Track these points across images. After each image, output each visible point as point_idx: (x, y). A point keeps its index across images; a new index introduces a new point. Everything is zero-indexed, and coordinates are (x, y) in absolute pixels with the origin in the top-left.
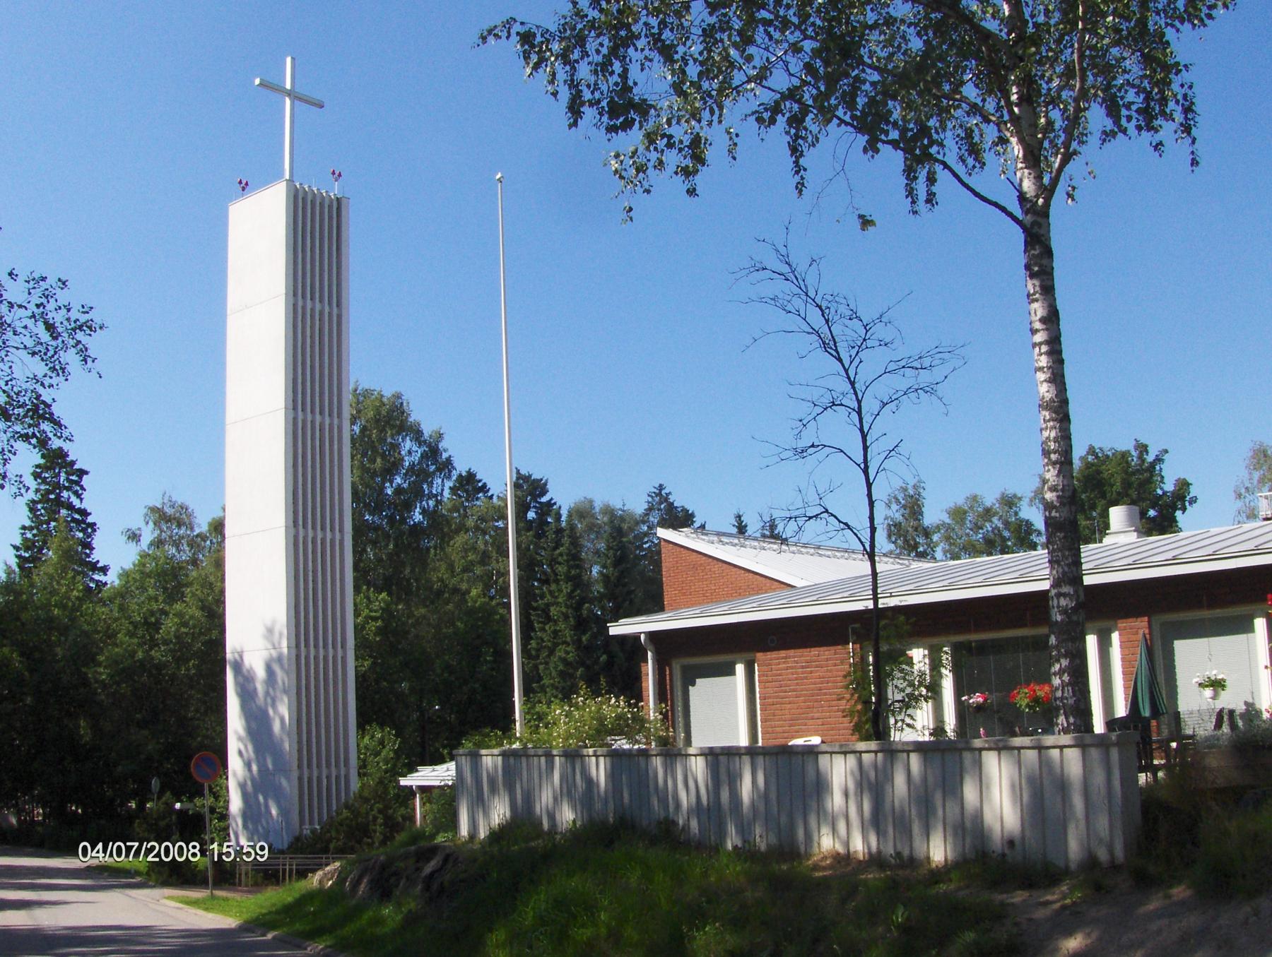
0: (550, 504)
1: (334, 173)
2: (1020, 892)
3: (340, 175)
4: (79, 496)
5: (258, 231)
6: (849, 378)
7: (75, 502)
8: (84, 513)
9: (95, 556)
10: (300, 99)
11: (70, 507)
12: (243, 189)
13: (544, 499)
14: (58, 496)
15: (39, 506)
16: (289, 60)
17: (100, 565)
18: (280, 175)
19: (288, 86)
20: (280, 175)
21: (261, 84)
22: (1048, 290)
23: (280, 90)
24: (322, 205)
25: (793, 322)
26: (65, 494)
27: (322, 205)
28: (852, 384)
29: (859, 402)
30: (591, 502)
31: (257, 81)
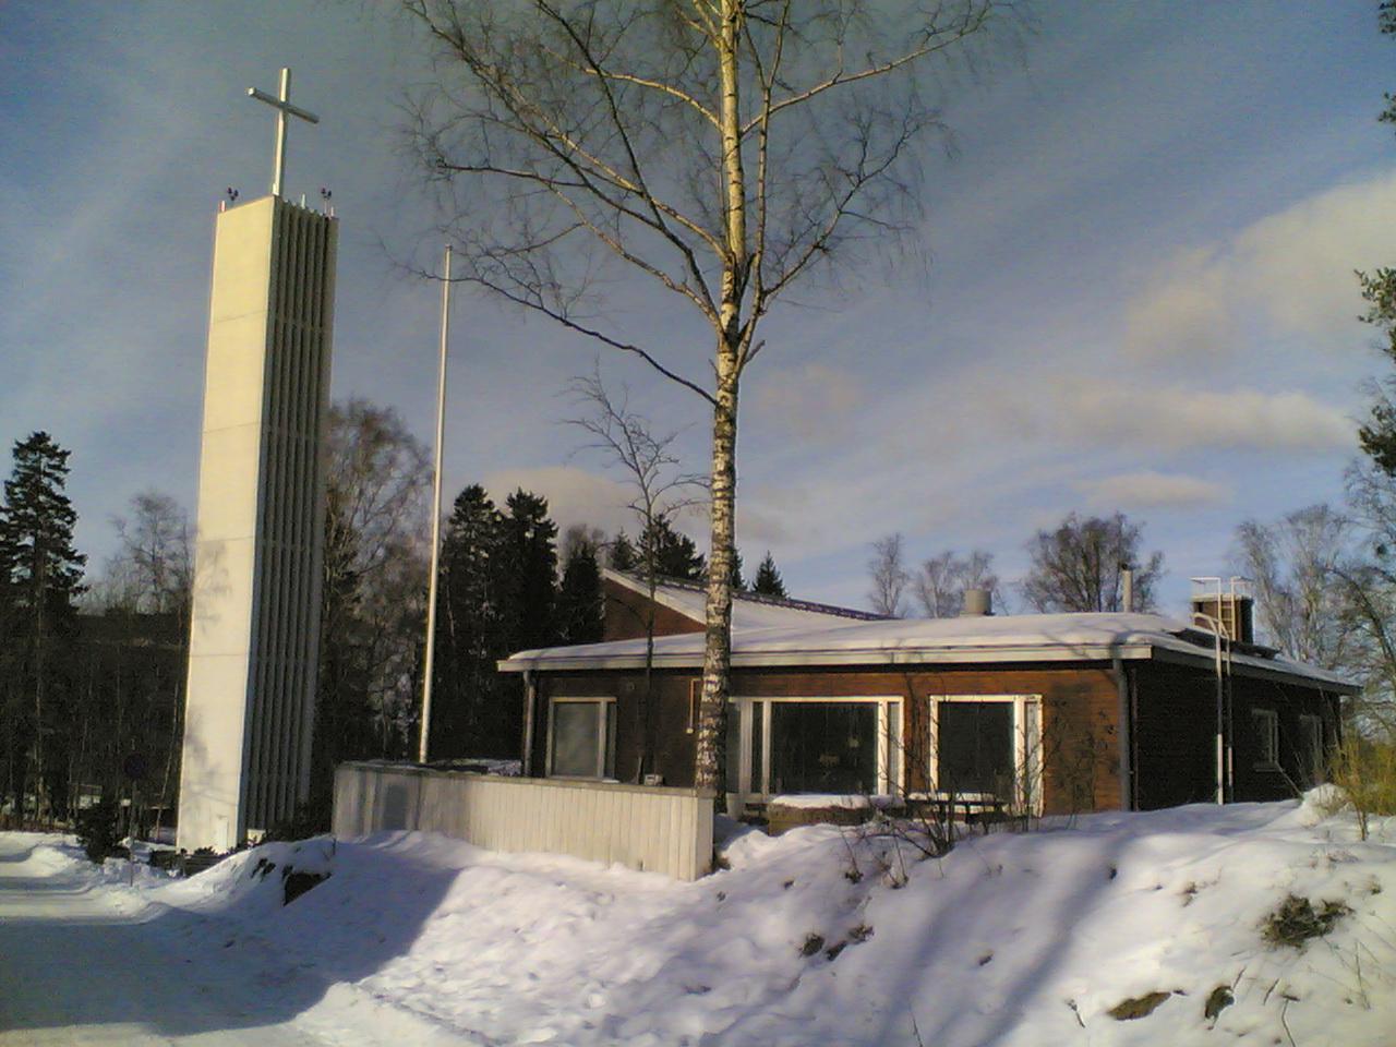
0: (547, 525)
1: (324, 192)
2: (1160, 842)
3: (330, 194)
4: (59, 481)
5: (244, 242)
6: (643, 485)
7: (56, 489)
8: (64, 501)
9: (72, 545)
10: (295, 113)
11: (50, 494)
12: (233, 199)
13: (542, 520)
14: (39, 481)
15: (17, 490)
16: (285, 71)
17: (76, 555)
18: (268, 193)
19: (283, 99)
20: (268, 193)
21: (254, 95)
22: (729, 450)
23: (272, 101)
24: (309, 224)
25: (598, 438)
26: (46, 481)
27: (309, 224)
28: (645, 490)
29: (649, 506)
30: (585, 526)
31: (251, 91)
